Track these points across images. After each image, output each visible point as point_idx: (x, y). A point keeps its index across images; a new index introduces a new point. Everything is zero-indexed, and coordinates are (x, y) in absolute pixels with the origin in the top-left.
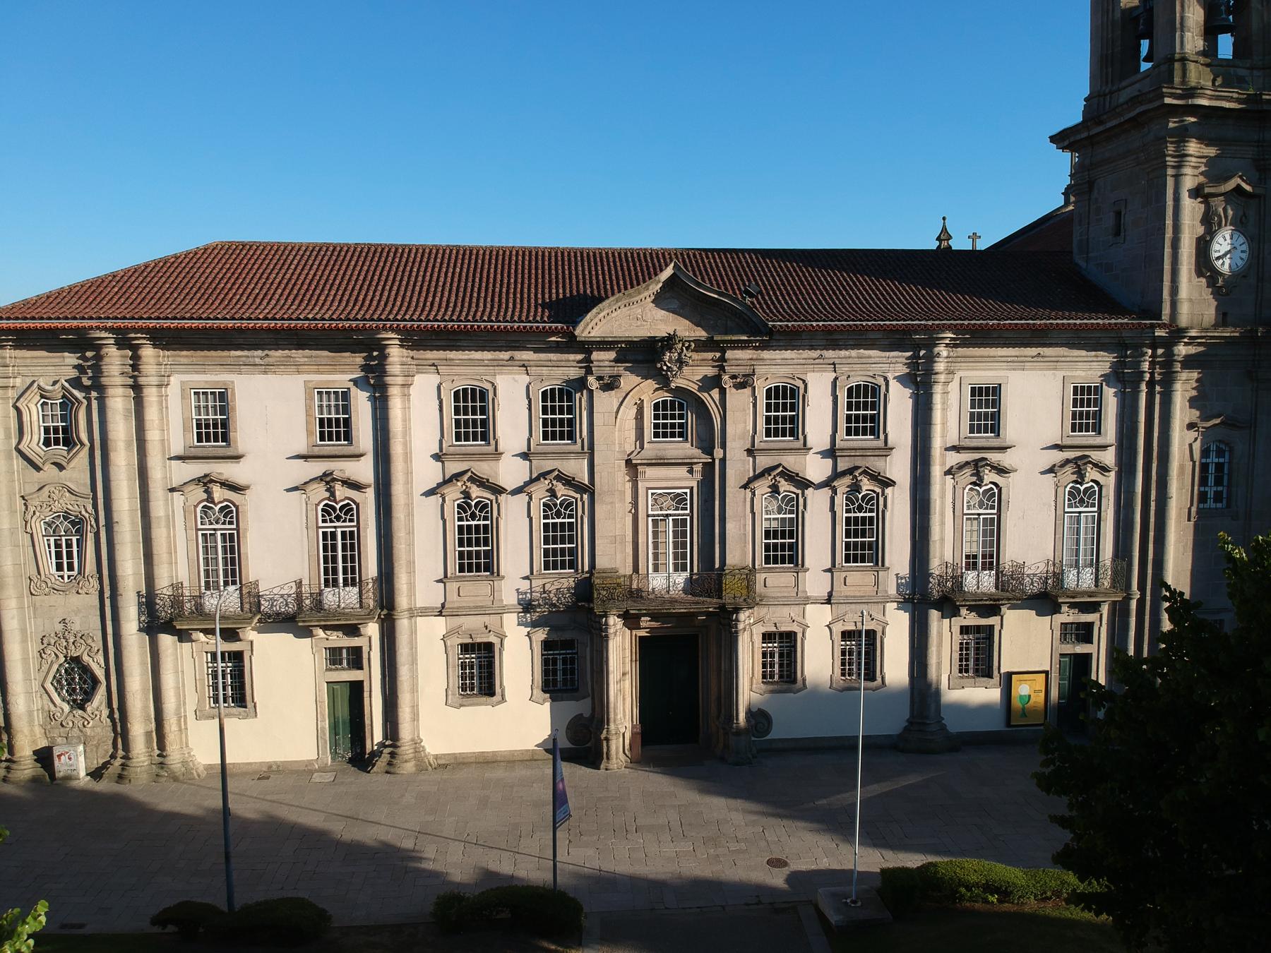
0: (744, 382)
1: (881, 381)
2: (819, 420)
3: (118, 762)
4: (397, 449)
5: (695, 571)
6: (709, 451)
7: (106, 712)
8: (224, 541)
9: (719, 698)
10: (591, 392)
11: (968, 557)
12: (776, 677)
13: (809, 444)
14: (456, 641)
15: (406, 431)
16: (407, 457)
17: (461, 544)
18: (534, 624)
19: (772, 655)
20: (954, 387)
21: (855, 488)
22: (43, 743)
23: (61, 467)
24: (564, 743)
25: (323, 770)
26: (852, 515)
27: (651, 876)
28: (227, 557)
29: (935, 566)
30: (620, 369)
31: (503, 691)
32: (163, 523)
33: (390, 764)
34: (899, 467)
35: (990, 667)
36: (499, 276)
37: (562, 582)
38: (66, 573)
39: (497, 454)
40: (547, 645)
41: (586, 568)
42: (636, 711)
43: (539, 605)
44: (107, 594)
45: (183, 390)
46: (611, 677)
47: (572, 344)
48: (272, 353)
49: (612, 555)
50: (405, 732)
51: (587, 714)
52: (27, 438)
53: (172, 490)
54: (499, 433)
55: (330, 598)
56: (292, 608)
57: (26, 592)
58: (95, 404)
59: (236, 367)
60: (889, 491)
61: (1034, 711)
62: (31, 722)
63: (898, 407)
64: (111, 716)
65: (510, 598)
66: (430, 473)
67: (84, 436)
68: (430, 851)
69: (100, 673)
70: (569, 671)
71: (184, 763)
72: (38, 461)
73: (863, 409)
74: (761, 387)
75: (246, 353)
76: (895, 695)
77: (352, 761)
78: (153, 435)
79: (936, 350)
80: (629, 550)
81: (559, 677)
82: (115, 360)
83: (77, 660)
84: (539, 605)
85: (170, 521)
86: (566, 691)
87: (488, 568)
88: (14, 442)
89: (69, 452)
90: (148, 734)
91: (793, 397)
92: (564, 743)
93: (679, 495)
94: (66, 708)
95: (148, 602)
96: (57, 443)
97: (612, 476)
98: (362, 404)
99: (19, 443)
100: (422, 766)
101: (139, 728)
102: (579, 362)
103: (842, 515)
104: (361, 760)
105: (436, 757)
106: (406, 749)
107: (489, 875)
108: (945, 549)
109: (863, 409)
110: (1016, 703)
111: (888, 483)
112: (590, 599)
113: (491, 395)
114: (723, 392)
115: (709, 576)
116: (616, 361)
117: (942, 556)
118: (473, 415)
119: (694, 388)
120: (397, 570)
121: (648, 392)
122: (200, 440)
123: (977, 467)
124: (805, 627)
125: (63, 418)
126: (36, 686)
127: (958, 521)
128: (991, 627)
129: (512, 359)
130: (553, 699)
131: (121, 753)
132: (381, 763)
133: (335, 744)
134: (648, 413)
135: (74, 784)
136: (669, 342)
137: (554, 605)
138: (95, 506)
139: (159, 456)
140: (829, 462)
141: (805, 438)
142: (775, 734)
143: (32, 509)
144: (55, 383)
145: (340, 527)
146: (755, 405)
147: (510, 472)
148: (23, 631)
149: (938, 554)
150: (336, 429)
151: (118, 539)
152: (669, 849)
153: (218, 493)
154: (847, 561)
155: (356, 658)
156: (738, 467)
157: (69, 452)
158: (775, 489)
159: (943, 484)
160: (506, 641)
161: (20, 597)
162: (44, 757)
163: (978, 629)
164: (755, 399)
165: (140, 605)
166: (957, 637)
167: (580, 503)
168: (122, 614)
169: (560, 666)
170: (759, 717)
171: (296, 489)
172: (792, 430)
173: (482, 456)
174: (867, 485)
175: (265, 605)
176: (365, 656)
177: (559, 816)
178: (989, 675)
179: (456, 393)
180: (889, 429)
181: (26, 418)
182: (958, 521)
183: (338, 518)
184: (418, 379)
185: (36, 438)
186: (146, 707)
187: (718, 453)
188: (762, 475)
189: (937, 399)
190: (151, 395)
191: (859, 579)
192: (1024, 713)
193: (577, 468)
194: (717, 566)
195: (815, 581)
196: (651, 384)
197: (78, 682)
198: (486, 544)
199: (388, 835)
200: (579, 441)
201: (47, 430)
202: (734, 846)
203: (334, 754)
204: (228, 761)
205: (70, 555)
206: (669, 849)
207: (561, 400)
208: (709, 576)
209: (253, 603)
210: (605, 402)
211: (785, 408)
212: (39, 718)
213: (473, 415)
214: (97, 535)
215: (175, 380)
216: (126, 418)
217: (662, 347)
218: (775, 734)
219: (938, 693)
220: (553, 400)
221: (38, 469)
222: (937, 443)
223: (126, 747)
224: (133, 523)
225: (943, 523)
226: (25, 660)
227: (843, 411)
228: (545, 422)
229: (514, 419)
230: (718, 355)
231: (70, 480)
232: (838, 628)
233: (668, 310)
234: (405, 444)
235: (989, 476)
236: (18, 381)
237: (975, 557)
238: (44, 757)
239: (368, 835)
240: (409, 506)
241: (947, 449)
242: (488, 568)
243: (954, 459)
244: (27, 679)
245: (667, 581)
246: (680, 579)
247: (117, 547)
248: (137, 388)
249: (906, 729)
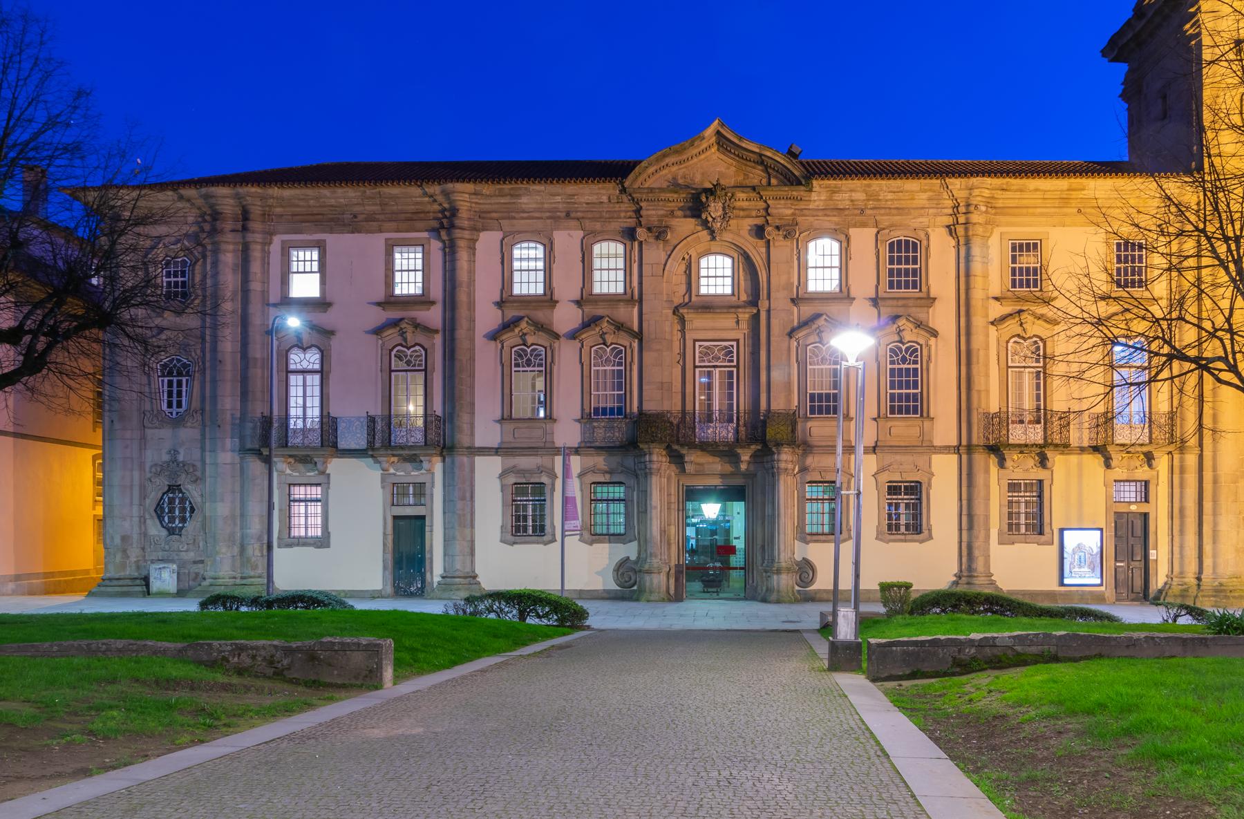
15: (471, 282)
16: (471, 306)
20: (994, 241)
26: (896, 366)
31: (930, 530)
34: (943, 317)
45: (283, 249)
50: (979, 565)
51: (633, 557)
91: (915, 250)
93: (726, 347)
154: (892, 412)
160: (934, 479)
167: (629, 351)
172: (914, 282)
180: (931, 282)
184: (483, 236)
187: (763, 304)
198: (916, 387)
204: (862, 587)
205: (179, 394)
216: (234, 271)
220: (899, 251)
222: (977, 295)
232: (885, 477)
243: (997, 310)
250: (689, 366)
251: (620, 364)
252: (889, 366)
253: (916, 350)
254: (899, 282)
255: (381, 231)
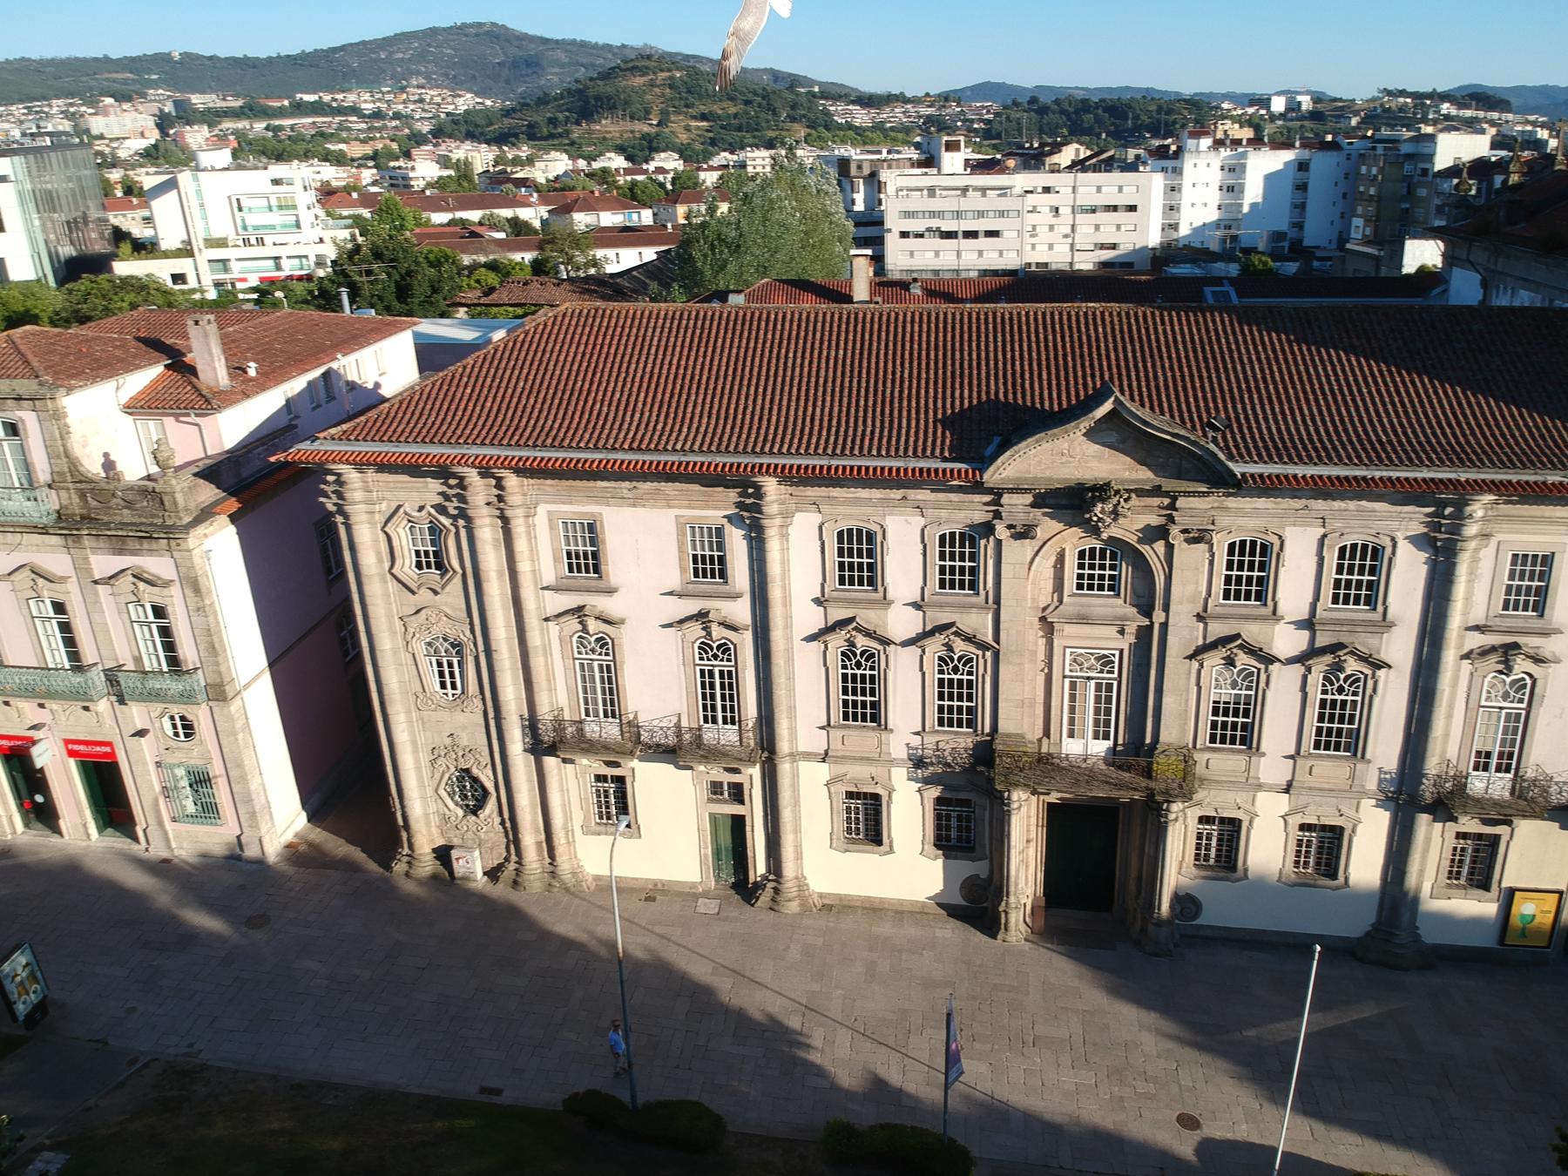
0: (1199, 537)
1: (1387, 542)
2: (1296, 583)
3: (512, 866)
4: (775, 593)
5: (1120, 741)
6: (1147, 611)
7: (497, 820)
8: (601, 671)
9: (1139, 878)
10: (999, 543)
11: (1479, 753)
12: (1212, 861)
13: (1280, 611)
14: (842, 789)
15: (785, 573)
17: (845, 692)
18: (927, 781)
19: (1209, 838)
21: (1338, 667)
22: (440, 842)
23: (436, 593)
24: (957, 899)
25: (706, 895)
26: (1329, 697)
27: (1047, 1117)
28: (607, 689)
29: (1432, 766)
30: (1038, 512)
32: (540, 652)
33: (773, 900)
34: (1399, 647)
35: (1489, 878)
36: (890, 365)
37: (960, 741)
38: (450, 691)
39: (886, 602)
40: (939, 801)
41: (987, 730)
42: (1041, 876)
43: (932, 764)
44: (491, 715)
45: (550, 520)
46: (1013, 852)
47: (978, 487)
48: (640, 485)
49: (1018, 719)
50: (789, 869)
51: (984, 875)
52: (398, 563)
53: (547, 619)
54: (888, 579)
55: (710, 734)
56: (672, 741)
57: (413, 707)
58: (463, 532)
59: (603, 499)
60: (1381, 673)
61: (1538, 932)
62: (428, 824)
63: (1408, 575)
64: (503, 823)
65: (900, 753)
66: (813, 619)
67: (455, 563)
68: (817, 1040)
69: (490, 786)
70: (967, 825)
71: (574, 874)
72: (413, 586)
73: (1361, 573)
74: (1221, 543)
75: (612, 484)
76: (1360, 897)
77: (734, 886)
78: (524, 567)
79: (1468, 509)
80: (1040, 711)
81: (953, 834)
82: (480, 491)
83: (467, 771)
84: (932, 764)
85: (547, 650)
86: (961, 849)
87: (875, 718)
88: (387, 565)
89: (442, 576)
90: (539, 844)
92: (957, 899)
93: (1105, 656)
94: (460, 812)
95: (532, 725)
96: (429, 566)
97: (1021, 630)
98: (737, 544)
99: (392, 567)
100: (806, 909)
101: (530, 838)
102: (986, 504)
103: (1316, 696)
104: (745, 889)
105: (821, 896)
106: (789, 885)
107: (878, 1085)
108: (1449, 745)
109: (1361, 573)
110: (1515, 920)
111: (1377, 665)
112: (990, 763)
113: (879, 539)
114: (1170, 548)
115: (1136, 751)
116: (1033, 505)
117: (1444, 752)
118: (858, 560)
119: (1132, 539)
120: (777, 716)
121: (1073, 541)
122: (571, 571)
123: (1508, 652)
124: (1253, 816)
125: (433, 543)
126: (430, 791)
127: (1472, 714)
128: (1497, 838)
129: (904, 498)
130: (946, 857)
131: (514, 858)
132: (765, 897)
133: (718, 869)
134: (1071, 563)
135: (472, 885)
136: (1101, 491)
137: (949, 765)
138: (472, 631)
139: (532, 587)
140: (1306, 634)
141: (1275, 604)
142: (1202, 920)
143: (411, 630)
144: (421, 509)
145: (718, 666)
146: (1211, 563)
147: (901, 622)
148: (414, 742)
149: (1438, 751)
150: (710, 567)
151: (497, 666)
152: (1069, 1079)
153: (593, 625)
155: (737, 794)
156: (1183, 633)
157: (442, 576)
158: (1230, 662)
159: (1458, 670)
160: (894, 795)
161: (408, 712)
162: (443, 854)
163: (1479, 836)
164: (1213, 555)
165: (523, 727)
166: (1451, 841)
167: (981, 661)
168: (507, 736)
169: (954, 823)
170: (1186, 903)
171: (670, 625)
173: (870, 603)
174: (1352, 666)
175: (645, 736)
176: (746, 792)
177: (952, 1076)
178: (1486, 887)
179: (840, 534)
180: (1390, 600)
181: (395, 543)
182: (1472, 714)
183: (715, 657)
184: (799, 517)
185: (407, 562)
186: (534, 821)
187: (1158, 616)
188: (1214, 645)
189: (1462, 570)
190: (519, 527)
191: (1330, 768)
192: (1524, 932)
193: (981, 624)
194: (1148, 741)
195: (1272, 763)
196: (1076, 532)
197: (472, 794)
199: (776, 1006)
200: (982, 592)
201: (418, 553)
202: (1142, 1086)
203: (718, 877)
205: (452, 675)
206: (1069, 1079)
207: (962, 545)
208: (1136, 751)
209: (632, 730)
210: (1017, 553)
211: (1252, 570)
212: (435, 820)
213: (858, 560)
214: (477, 658)
215: (542, 510)
216: (496, 547)
217: (1093, 497)
218: (1202, 920)
219: (1416, 900)
221: (413, 593)
222: (1455, 622)
223: (519, 853)
224: (511, 650)
225: (1450, 716)
226: (418, 768)
227: (1330, 574)
228: (942, 570)
229: (905, 563)
230: (1167, 501)
231: (446, 604)
232: (1296, 820)
233: (1104, 445)
234: (784, 587)
235: (1521, 666)
236: (384, 506)
237: (1488, 755)
238: (443, 854)
239: (756, 1003)
240: (789, 651)
241: (1468, 629)
242: (875, 718)
243: (1476, 641)
244: (421, 786)
245: (1086, 747)
246: (1100, 747)
247: (498, 674)
248: (505, 520)
249: (1368, 934)
250: (1473, 704)
251: (1249, 688)
252: (1320, 696)
253: (873, 655)
254: (1517, 602)
255: (669, 507)
